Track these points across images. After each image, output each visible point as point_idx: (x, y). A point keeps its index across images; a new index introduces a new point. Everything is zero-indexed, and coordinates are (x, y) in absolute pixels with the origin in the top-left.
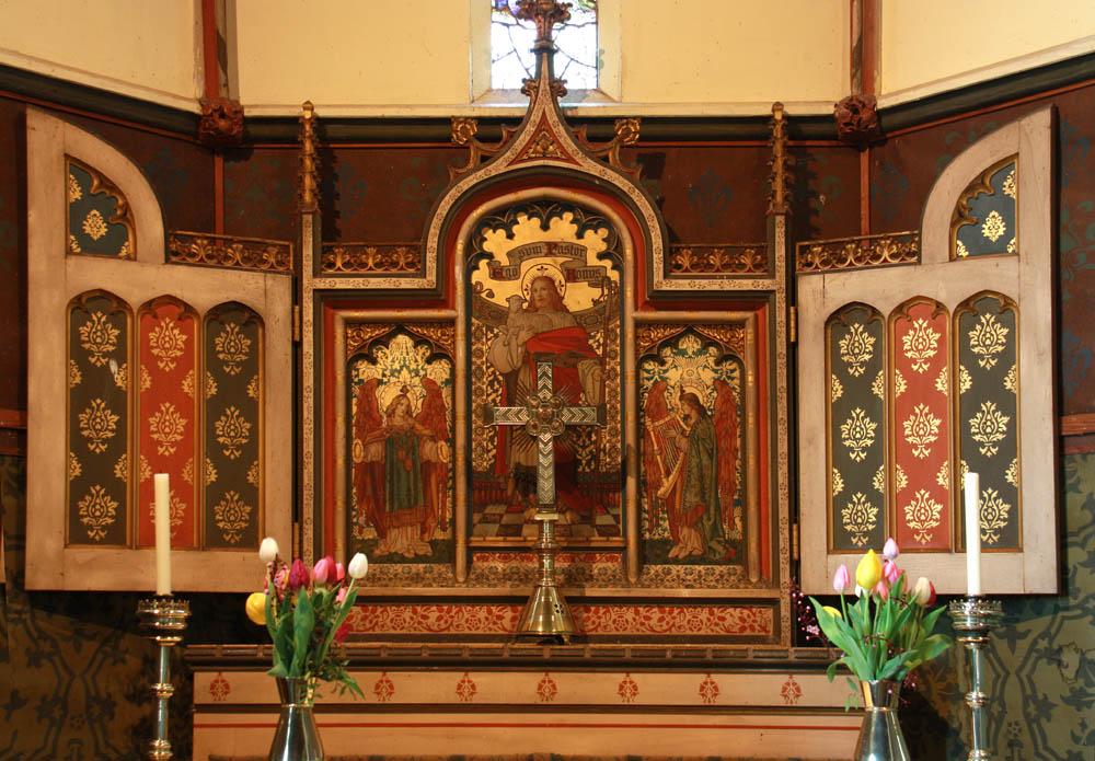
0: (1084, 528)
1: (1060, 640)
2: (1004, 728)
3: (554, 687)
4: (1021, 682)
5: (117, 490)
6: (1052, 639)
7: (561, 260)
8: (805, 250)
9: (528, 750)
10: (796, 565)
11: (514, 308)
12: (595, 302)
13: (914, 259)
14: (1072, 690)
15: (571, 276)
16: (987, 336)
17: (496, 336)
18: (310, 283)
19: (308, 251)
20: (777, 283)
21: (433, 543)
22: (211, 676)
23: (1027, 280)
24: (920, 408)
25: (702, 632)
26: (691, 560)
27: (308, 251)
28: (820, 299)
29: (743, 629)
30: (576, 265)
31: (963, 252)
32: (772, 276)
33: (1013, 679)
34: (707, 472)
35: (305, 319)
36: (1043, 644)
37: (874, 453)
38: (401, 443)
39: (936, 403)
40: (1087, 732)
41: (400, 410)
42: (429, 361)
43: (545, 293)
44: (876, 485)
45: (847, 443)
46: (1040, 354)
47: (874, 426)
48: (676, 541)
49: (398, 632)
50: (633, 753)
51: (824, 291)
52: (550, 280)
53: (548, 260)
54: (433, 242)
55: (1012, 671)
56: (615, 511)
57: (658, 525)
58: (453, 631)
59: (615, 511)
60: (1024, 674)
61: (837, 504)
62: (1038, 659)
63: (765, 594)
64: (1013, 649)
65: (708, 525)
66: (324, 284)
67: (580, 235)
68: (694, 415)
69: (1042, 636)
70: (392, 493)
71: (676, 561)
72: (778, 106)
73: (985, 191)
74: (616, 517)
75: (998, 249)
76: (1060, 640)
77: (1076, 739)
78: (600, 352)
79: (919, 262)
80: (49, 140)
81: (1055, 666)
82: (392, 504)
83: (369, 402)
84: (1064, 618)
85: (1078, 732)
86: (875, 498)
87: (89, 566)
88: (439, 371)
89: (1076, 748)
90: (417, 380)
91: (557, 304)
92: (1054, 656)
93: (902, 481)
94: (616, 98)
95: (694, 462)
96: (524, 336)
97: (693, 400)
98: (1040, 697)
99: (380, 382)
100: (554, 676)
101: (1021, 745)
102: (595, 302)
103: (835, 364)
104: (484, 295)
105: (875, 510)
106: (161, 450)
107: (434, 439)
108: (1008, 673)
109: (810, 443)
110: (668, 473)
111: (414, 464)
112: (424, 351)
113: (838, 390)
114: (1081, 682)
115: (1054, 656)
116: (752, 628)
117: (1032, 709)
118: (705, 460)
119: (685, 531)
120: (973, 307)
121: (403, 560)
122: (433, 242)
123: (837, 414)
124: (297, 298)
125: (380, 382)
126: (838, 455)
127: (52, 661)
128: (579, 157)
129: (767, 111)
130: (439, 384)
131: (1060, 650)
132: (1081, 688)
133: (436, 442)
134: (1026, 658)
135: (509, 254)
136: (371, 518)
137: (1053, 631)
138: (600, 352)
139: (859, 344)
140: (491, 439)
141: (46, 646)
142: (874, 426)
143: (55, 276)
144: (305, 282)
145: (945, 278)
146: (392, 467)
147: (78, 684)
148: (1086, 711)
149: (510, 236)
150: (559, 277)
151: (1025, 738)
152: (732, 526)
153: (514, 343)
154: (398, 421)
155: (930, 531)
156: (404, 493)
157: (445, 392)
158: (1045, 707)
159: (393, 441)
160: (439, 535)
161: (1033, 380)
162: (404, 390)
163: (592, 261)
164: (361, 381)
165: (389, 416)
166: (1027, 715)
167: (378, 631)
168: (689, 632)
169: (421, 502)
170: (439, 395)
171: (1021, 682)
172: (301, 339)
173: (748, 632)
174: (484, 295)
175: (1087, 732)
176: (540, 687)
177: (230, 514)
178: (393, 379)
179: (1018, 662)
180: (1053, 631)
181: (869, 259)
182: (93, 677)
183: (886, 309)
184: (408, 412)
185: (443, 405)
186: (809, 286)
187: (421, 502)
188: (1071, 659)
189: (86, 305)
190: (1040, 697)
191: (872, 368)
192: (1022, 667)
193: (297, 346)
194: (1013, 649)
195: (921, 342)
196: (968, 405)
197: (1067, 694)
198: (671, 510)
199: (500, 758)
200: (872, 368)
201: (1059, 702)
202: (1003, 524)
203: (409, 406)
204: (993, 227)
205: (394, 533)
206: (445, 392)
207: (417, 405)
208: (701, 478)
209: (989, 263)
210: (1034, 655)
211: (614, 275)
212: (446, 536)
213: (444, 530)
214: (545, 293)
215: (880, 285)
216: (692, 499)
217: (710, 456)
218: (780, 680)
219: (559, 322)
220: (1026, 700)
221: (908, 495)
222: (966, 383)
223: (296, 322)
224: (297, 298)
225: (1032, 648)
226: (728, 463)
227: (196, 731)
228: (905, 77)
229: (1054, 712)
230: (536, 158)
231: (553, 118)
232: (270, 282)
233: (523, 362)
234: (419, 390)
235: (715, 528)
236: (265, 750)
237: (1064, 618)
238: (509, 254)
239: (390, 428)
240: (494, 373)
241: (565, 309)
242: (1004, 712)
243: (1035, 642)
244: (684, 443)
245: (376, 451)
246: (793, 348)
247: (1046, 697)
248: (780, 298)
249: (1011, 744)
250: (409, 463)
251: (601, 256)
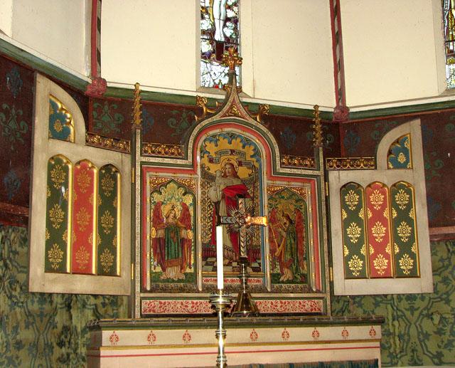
0: (440, 268)
1: (432, 310)
2: (410, 345)
3: (257, 335)
4: (417, 327)
5: (413, 256)
6: (428, 310)
7: (236, 157)
8: (329, 161)
9: (248, 363)
10: (332, 283)
11: (218, 175)
12: (250, 175)
13: (373, 168)
14: (438, 329)
15: (240, 164)
16: (402, 198)
17: (211, 186)
18: (139, 158)
19: (138, 145)
20: (321, 173)
21: (186, 274)
22: (111, 332)
23: (416, 177)
24: (404, 223)
25: (297, 311)
26: (288, 282)
27: (138, 145)
28: (338, 180)
29: (312, 310)
30: (242, 160)
31: (391, 166)
32: (319, 170)
33: (413, 326)
34: (293, 246)
35: (137, 174)
36: (425, 312)
37: (361, 241)
38: (172, 230)
39: (384, 223)
40: (444, 344)
41: (172, 215)
42: (184, 194)
43: (230, 170)
44: (362, 252)
45: (350, 236)
46: (423, 205)
47: (360, 229)
48: (283, 274)
49: (175, 313)
50: (321, 361)
51: (339, 177)
52: (232, 165)
53: (232, 157)
54: (190, 146)
55: (412, 322)
56: (259, 261)
57: (276, 267)
58: (198, 313)
59: (259, 261)
60: (417, 324)
61: (347, 259)
62: (423, 318)
63: (321, 295)
64: (412, 314)
65: (294, 267)
66: (144, 159)
67: (244, 147)
68: (288, 222)
69: (424, 309)
70: (168, 251)
71: (283, 282)
72: (316, 107)
73: (399, 147)
74: (259, 264)
75: (404, 166)
76: (432, 310)
77: (439, 347)
78: (252, 195)
79: (376, 168)
80: (44, 87)
81: (430, 320)
82: (168, 256)
83: (159, 212)
84: (433, 302)
85: (440, 344)
86: (362, 257)
87: (53, 281)
88: (188, 200)
89: (439, 350)
90: (178, 203)
91: (235, 175)
92: (430, 316)
93: (372, 251)
94: (251, 96)
95: (289, 241)
96: (222, 187)
97: (288, 217)
98: (425, 332)
99: (163, 203)
100: (256, 330)
101: (417, 351)
102: (250, 175)
103: (344, 206)
104: (206, 169)
105: (362, 262)
106: (80, 229)
107: (186, 229)
108: (411, 324)
109: (336, 235)
110: (279, 246)
111: (178, 239)
112: (182, 190)
113: (345, 216)
114: (441, 326)
115: (430, 316)
116: (315, 309)
117: (421, 337)
118: (293, 242)
119: (286, 270)
120: (397, 187)
121: (173, 281)
122: (190, 146)
123: (346, 224)
124: (134, 165)
125: (163, 203)
126: (346, 241)
127: (33, 326)
128: (248, 117)
129: (312, 108)
130: (188, 204)
131: (432, 314)
132: (27, 327)
133: (187, 230)
134: (418, 318)
135: (216, 153)
136: (159, 262)
137: (429, 307)
138: (252, 195)
139: (352, 199)
140: (210, 229)
141: (31, 320)
142: (360, 229)
143: (44, 148)
144: (137, 158)
145: (386, 176)
146: (168, 240)
147: (41, 337)
148: (443, 336)
149: (217, 146)
150: (236, 164)
151: (419, 348)
152: (303, 269)
153: (218, 190)
154: (170, 220)
155: (384, 270)
156: (173, 251)
157: (191, 209)
158: (427, 336)
159: (168, 229)
160: (188, 270)
161: (421, 213)
162: (173, 208)
163: (248, 158)
164: (155, 202)
165: (167, 218)
166: (419, 339)
167: (166, 313)
168: (172, 313)
169: (180, 256)
170: (188, 210)
171: (417, 327)
172: (135, 182)
173: (314, 311)
174: (206, 169)
175: (444, 344)
176: (251, 335)
177: (406, 263)
178: (168, 202)
179: (414, 320)
180: (429, 307)
181: (354, 166)
182: (46, 334)
183: (364, 185)
184: (175, 217)
185: (189, 214)
186: (333, 175)
187: (180, 256)
188: (436, 318)
189: (142, 163)
190: (425, 332)
191: (359, 207)
192: (417, 321)
193: (133, 185)
194: (412, 314)
195: (377, 199)
196: (396, 223)
197: (436, 330)
198: (280, 261)
199: (239, 366)
200: (359, 207)
201: (432, 333)
202: (411, 267)
203: (175, 214)
204: (402, 159)
205: (169, 269)
206: (191, 209)
207: (179, 215)
208: (291, 248)
209: (403, 173)
210: (421, 316)
211: (257, 165)
212: (192, 270)
213: (190, 268)
214: (230, 170)
215: (361, 176)
216: (288, 257)
217: (294, 240)
218: (341, 329)
219: (236, 182)
220: (419, 333)
221: (375, 256)
222: (370, 215)
223: (133, 175)
224: (134, 165)
225: (421, 314)
226: (301, 242)
227: (101, 359)
228: (360, 98)
229: (431, 337)
230: (231, 116)
231: (237, 101)
232: (124, 157)
233: (222, 198)
234: (180, 207)
235: (297, 269)
236: (214, 364)
237: (433, 302)
238: (216, 153)
239: (168, 223)
240: (210, 202)
241: (238, 177)
242: (409, 340)
243: (422, 311)
244: (284, 234)
245: (161, 233)
246: (327, 198)
247: (427, 333)
248: (322, 178)
249: (413, 351)
250: (175, 238)
251: (252, 156)
